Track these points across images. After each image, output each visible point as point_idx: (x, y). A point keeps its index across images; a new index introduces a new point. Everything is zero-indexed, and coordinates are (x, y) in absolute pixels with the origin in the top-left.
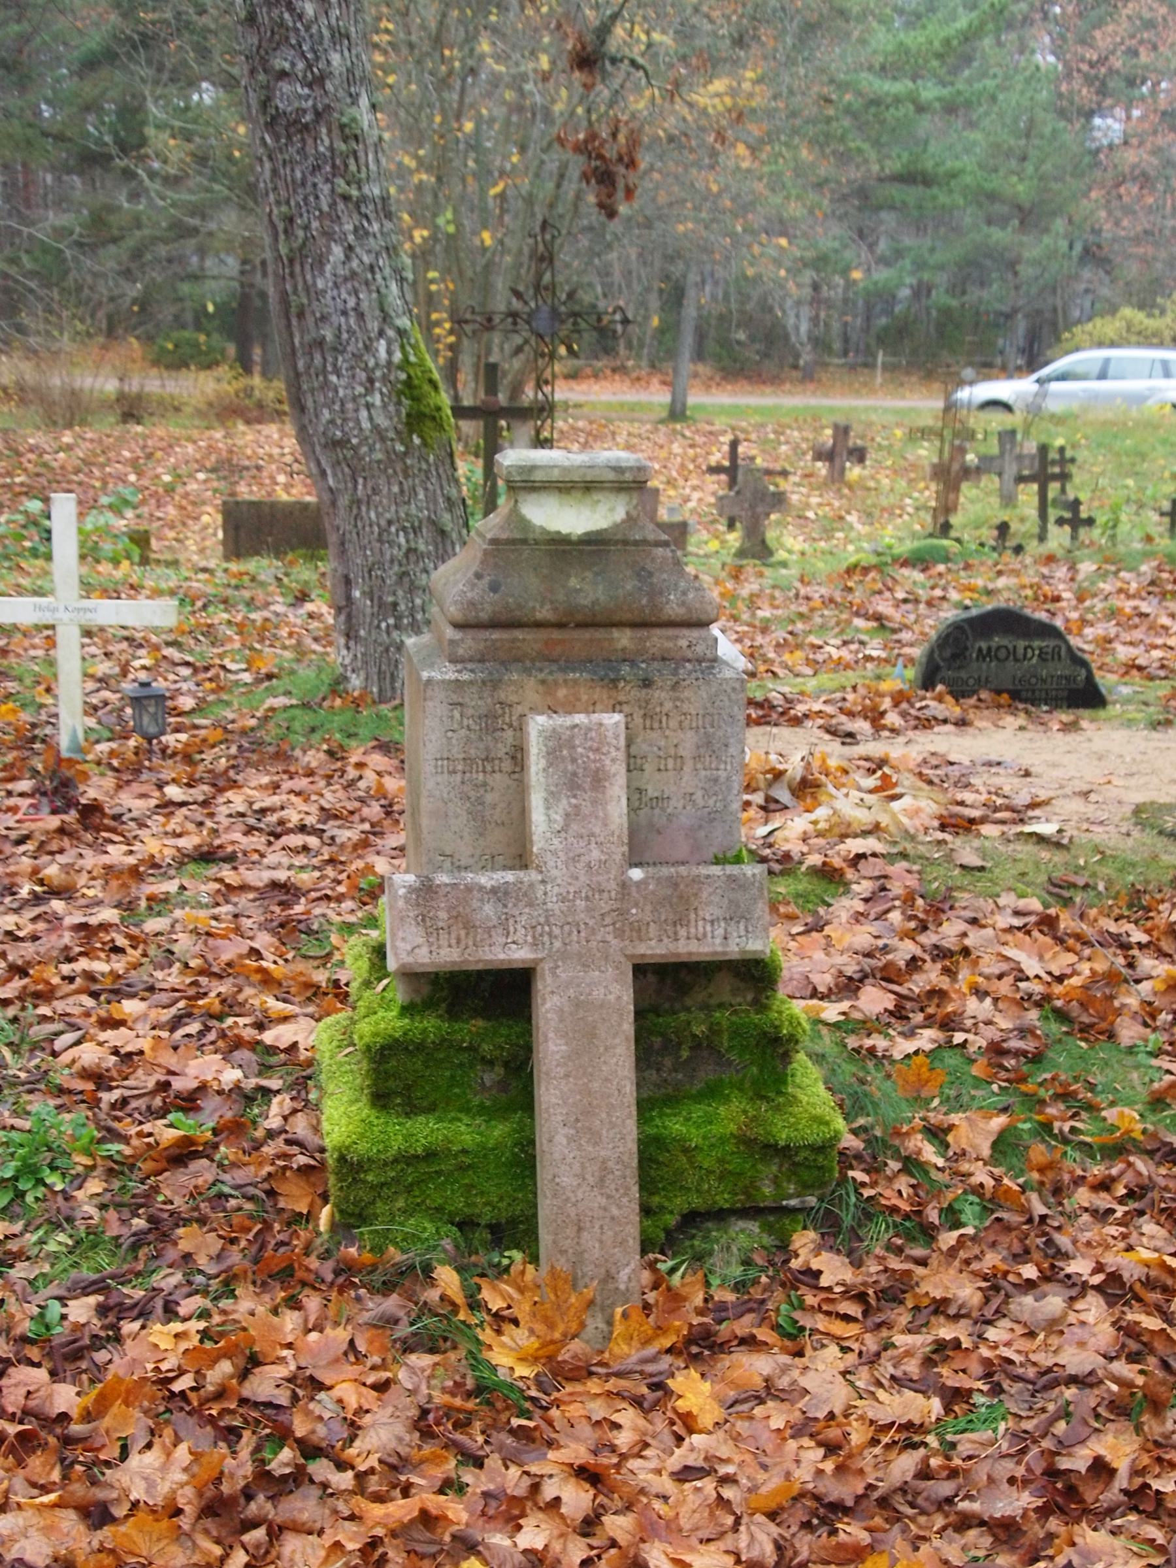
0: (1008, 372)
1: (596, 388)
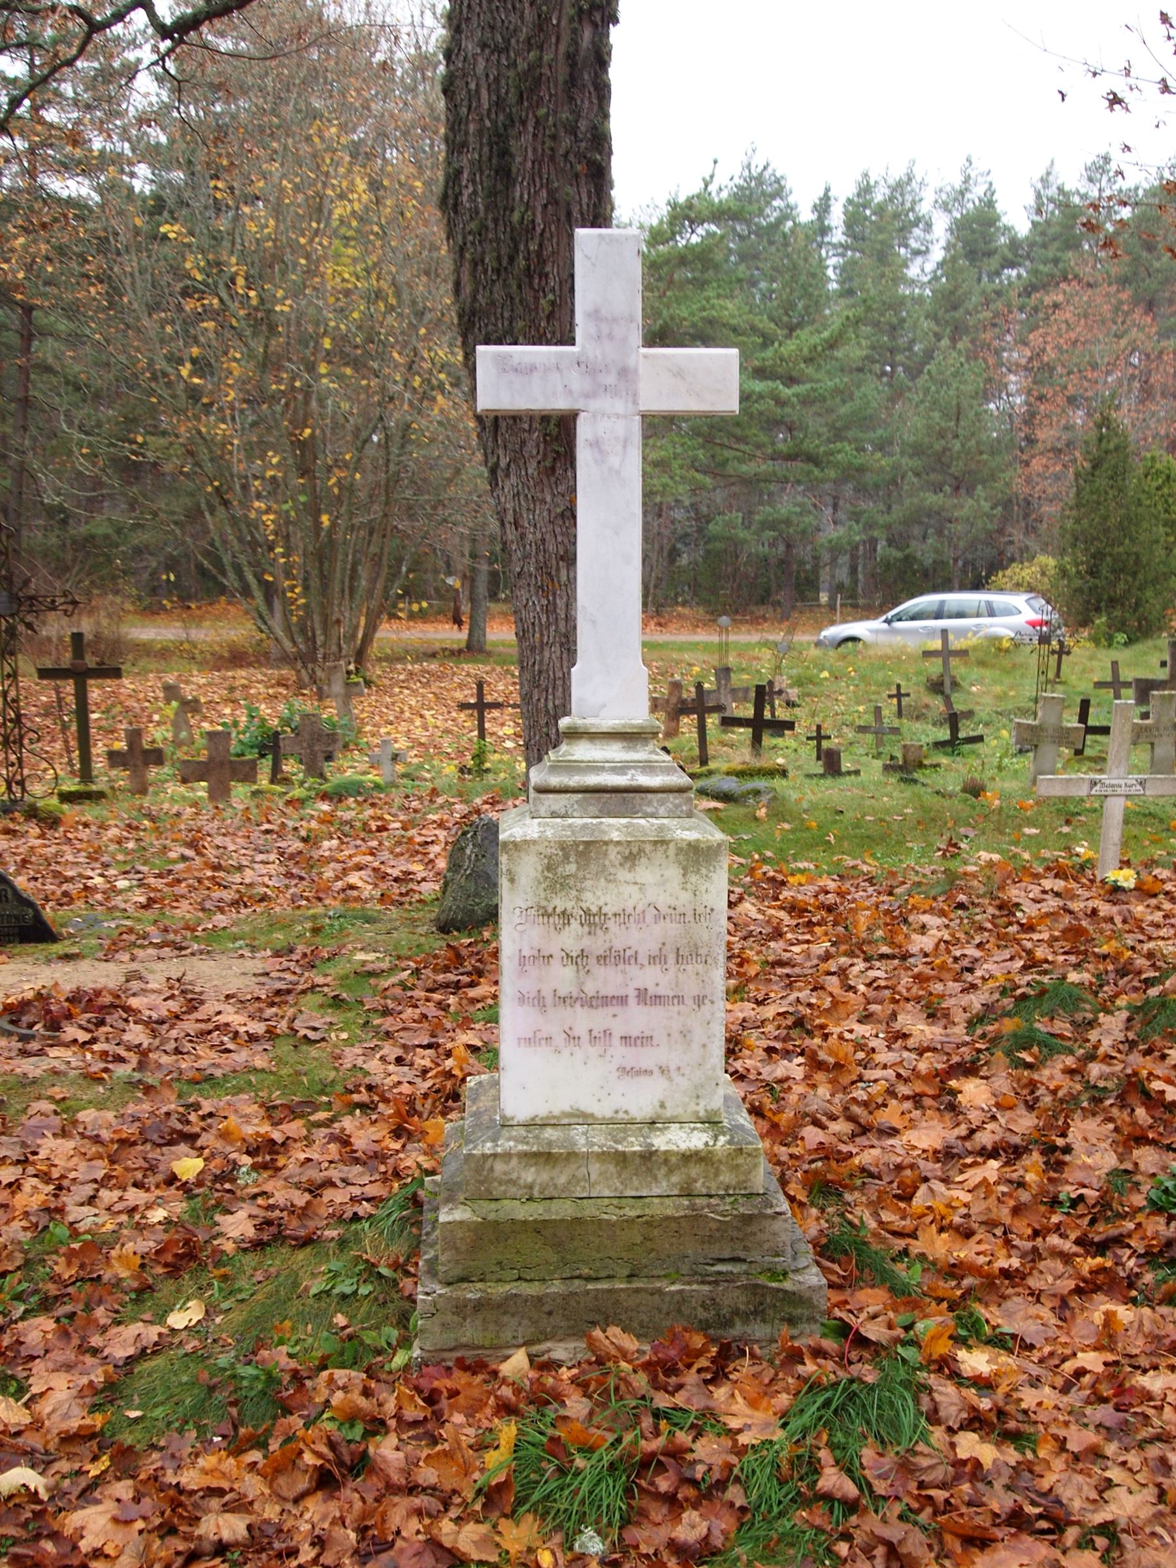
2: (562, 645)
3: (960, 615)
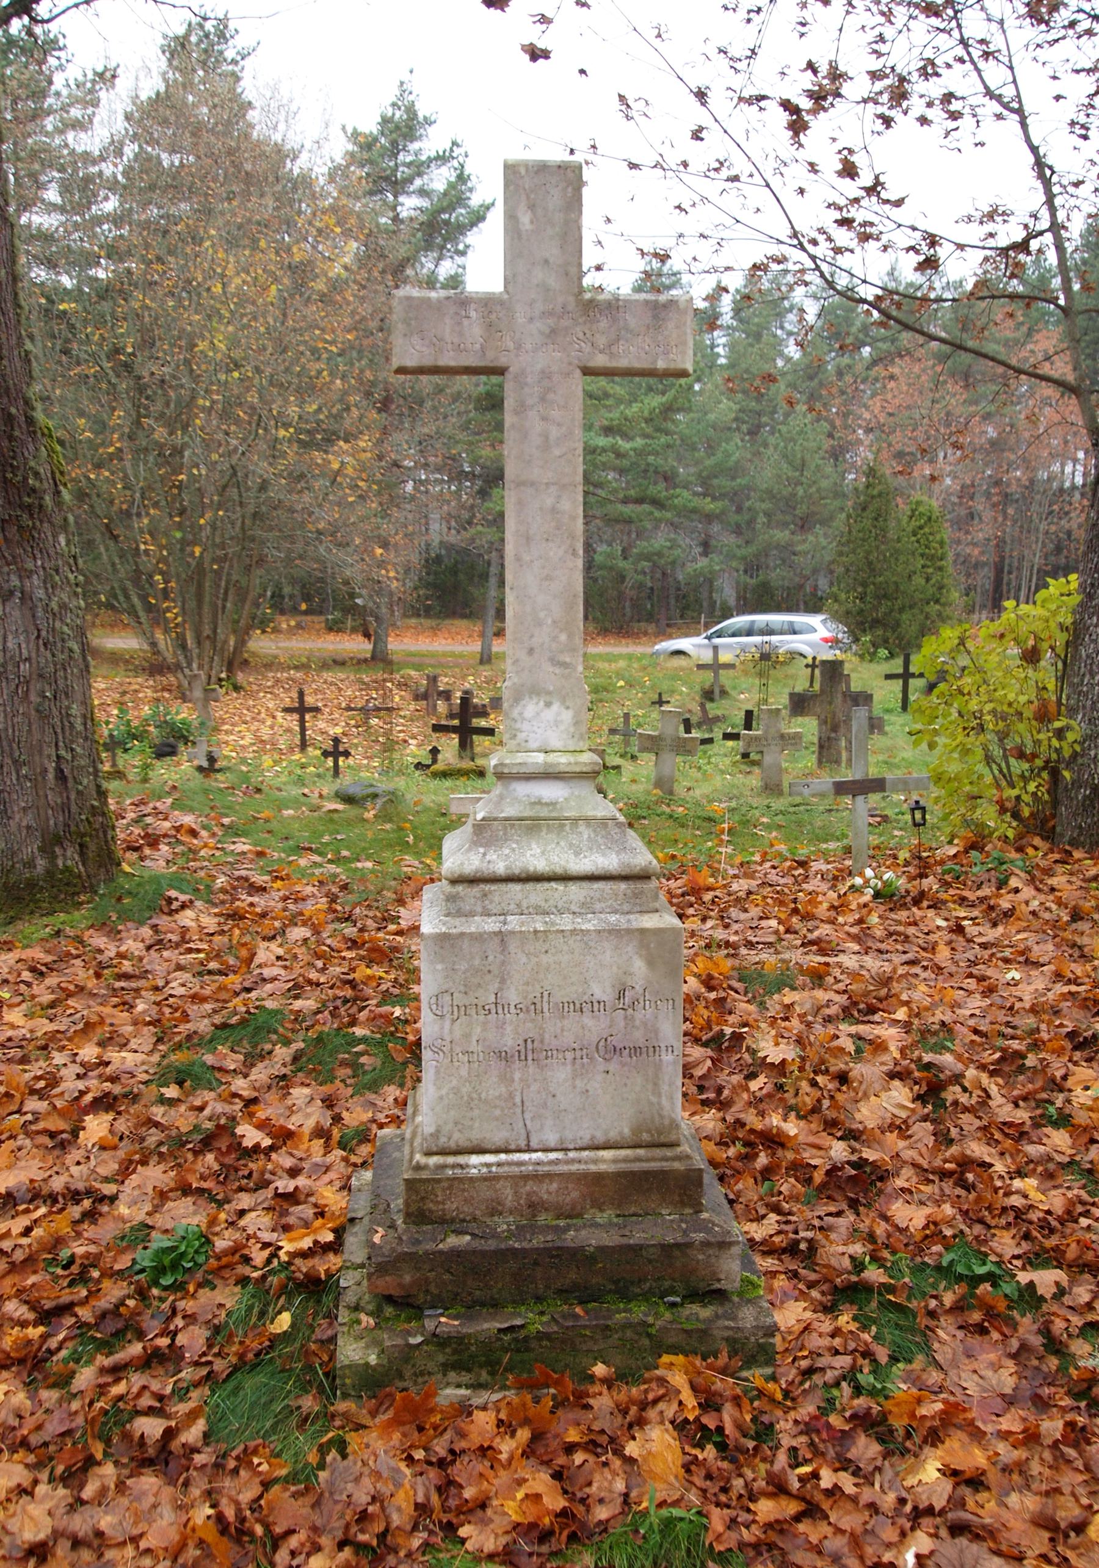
3: (771, 632)
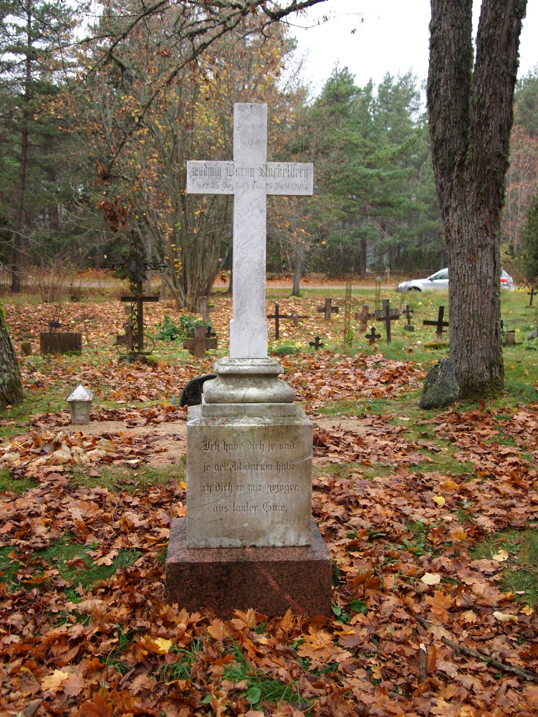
0: (418, 277)
1: (278, 283)
2: (478, 284)
